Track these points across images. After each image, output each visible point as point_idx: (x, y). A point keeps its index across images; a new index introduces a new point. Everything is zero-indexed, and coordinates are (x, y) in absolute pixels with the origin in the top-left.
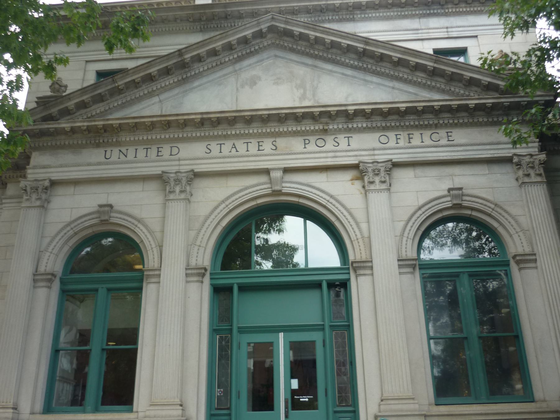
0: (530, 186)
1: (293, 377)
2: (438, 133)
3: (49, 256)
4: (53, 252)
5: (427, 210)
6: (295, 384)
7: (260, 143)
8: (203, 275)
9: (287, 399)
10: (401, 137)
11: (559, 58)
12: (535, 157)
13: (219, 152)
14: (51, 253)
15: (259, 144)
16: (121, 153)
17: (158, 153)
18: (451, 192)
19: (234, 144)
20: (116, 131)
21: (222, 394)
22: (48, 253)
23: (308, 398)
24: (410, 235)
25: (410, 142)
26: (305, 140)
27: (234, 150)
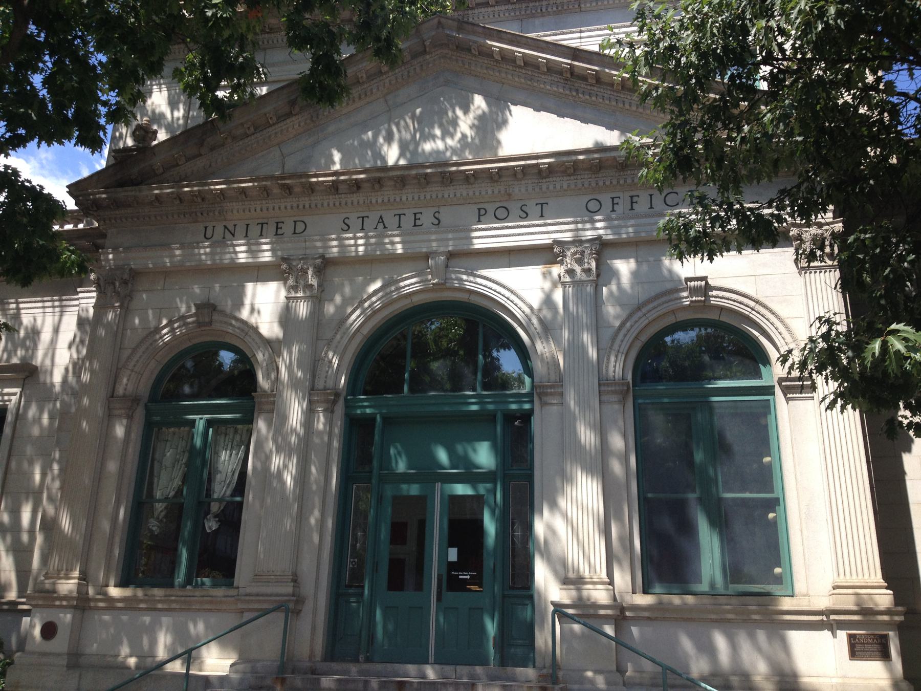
0: (808, 273)
1: (451, 545)
2: (677, 193)
3: (130, 375)
4: (135, 370)
5: (650, 311)
6: (453, 555)
7: (417, 215)
8: (334, 402)
9: (442, 575)
10: (620, 201)
11: (917, 73)
12: (825, 228)
13: (413, 224)
14: (132, 371)
15: (613, 201)
16: (226, 230)
17: (277, 231)
18: (689, 283)
19: (381, 217)
20: (218, 199)
21: (356, 566)
22: (129, 371)
23: (470, 575)
24: (623, 347)
25: (632, 209)
26: (479, 209)
27: (381, 226)
